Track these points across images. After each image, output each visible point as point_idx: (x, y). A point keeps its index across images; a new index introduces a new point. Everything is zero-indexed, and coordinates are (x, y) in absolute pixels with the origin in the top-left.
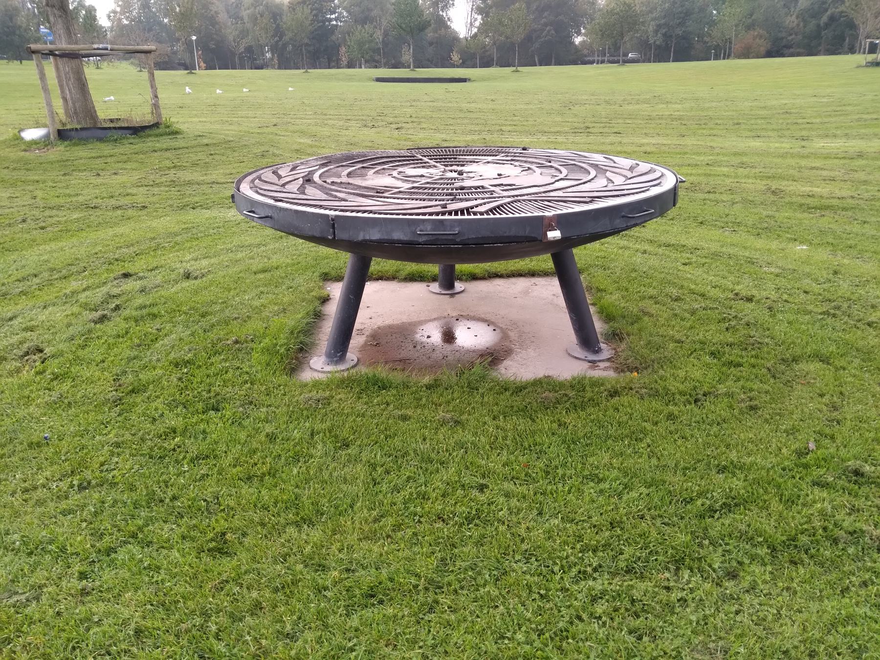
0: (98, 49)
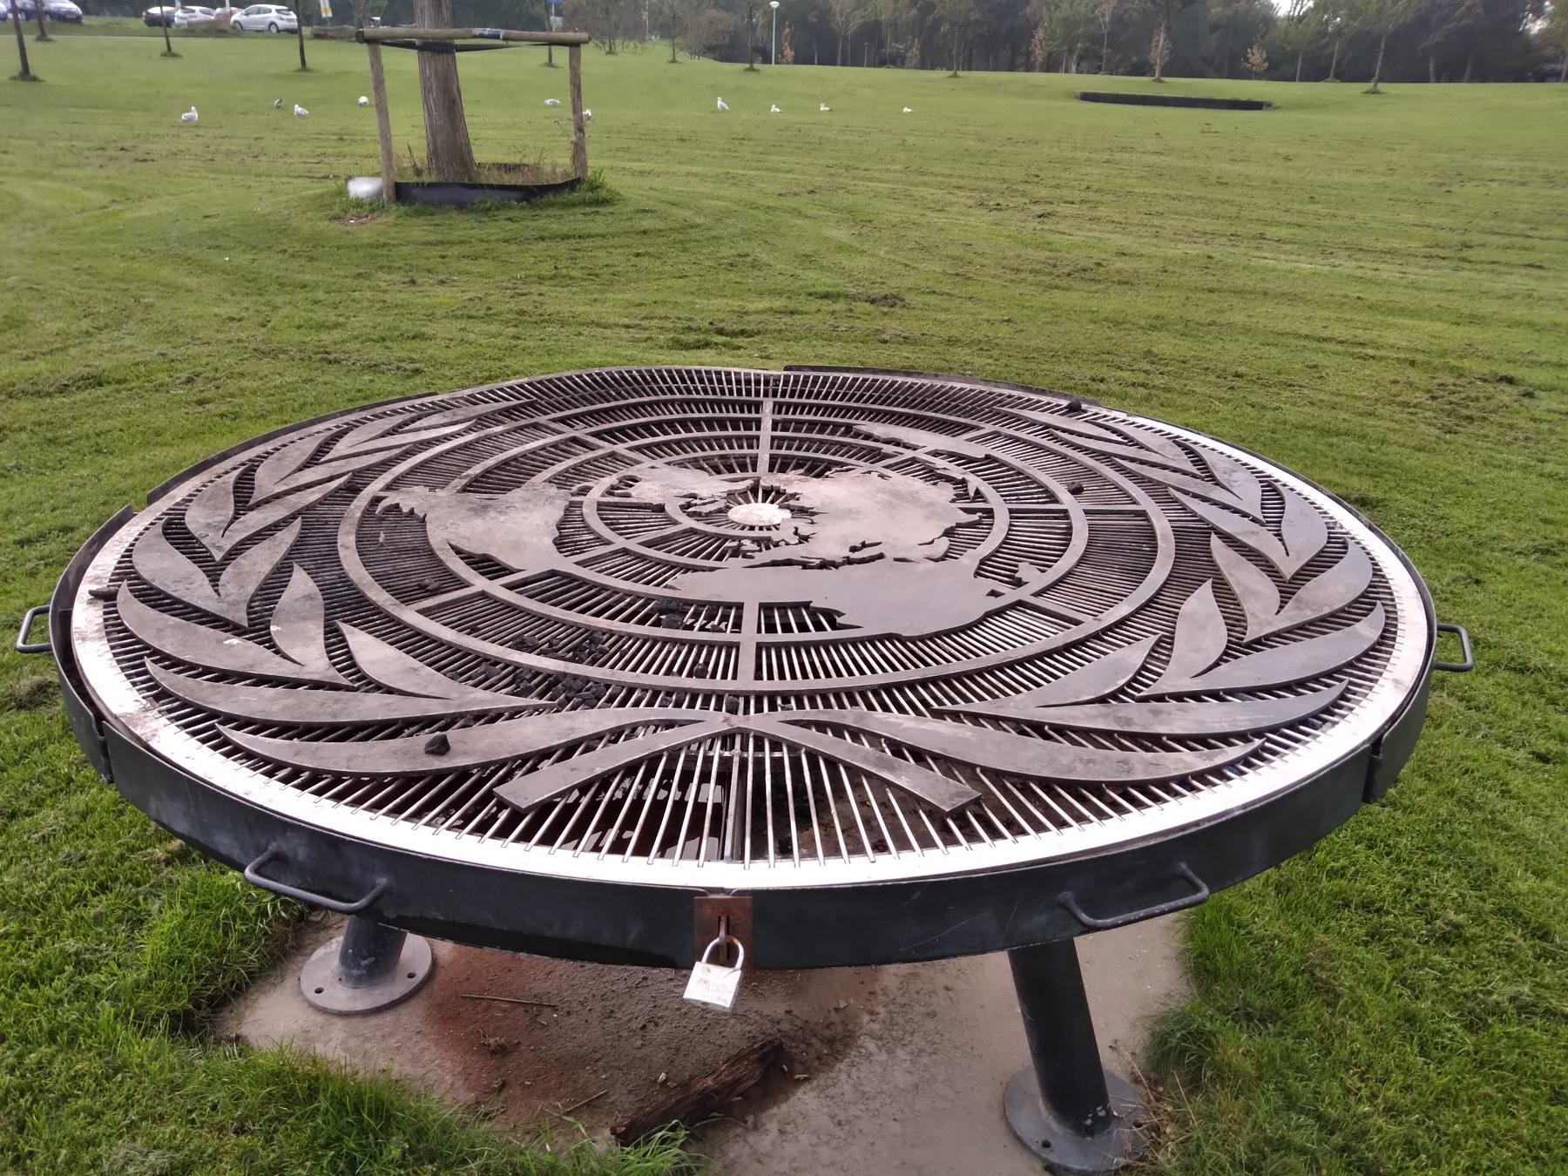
0: (482, 36)
